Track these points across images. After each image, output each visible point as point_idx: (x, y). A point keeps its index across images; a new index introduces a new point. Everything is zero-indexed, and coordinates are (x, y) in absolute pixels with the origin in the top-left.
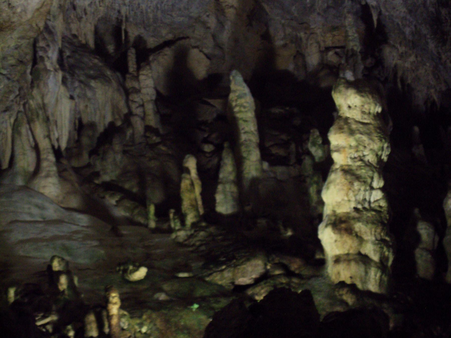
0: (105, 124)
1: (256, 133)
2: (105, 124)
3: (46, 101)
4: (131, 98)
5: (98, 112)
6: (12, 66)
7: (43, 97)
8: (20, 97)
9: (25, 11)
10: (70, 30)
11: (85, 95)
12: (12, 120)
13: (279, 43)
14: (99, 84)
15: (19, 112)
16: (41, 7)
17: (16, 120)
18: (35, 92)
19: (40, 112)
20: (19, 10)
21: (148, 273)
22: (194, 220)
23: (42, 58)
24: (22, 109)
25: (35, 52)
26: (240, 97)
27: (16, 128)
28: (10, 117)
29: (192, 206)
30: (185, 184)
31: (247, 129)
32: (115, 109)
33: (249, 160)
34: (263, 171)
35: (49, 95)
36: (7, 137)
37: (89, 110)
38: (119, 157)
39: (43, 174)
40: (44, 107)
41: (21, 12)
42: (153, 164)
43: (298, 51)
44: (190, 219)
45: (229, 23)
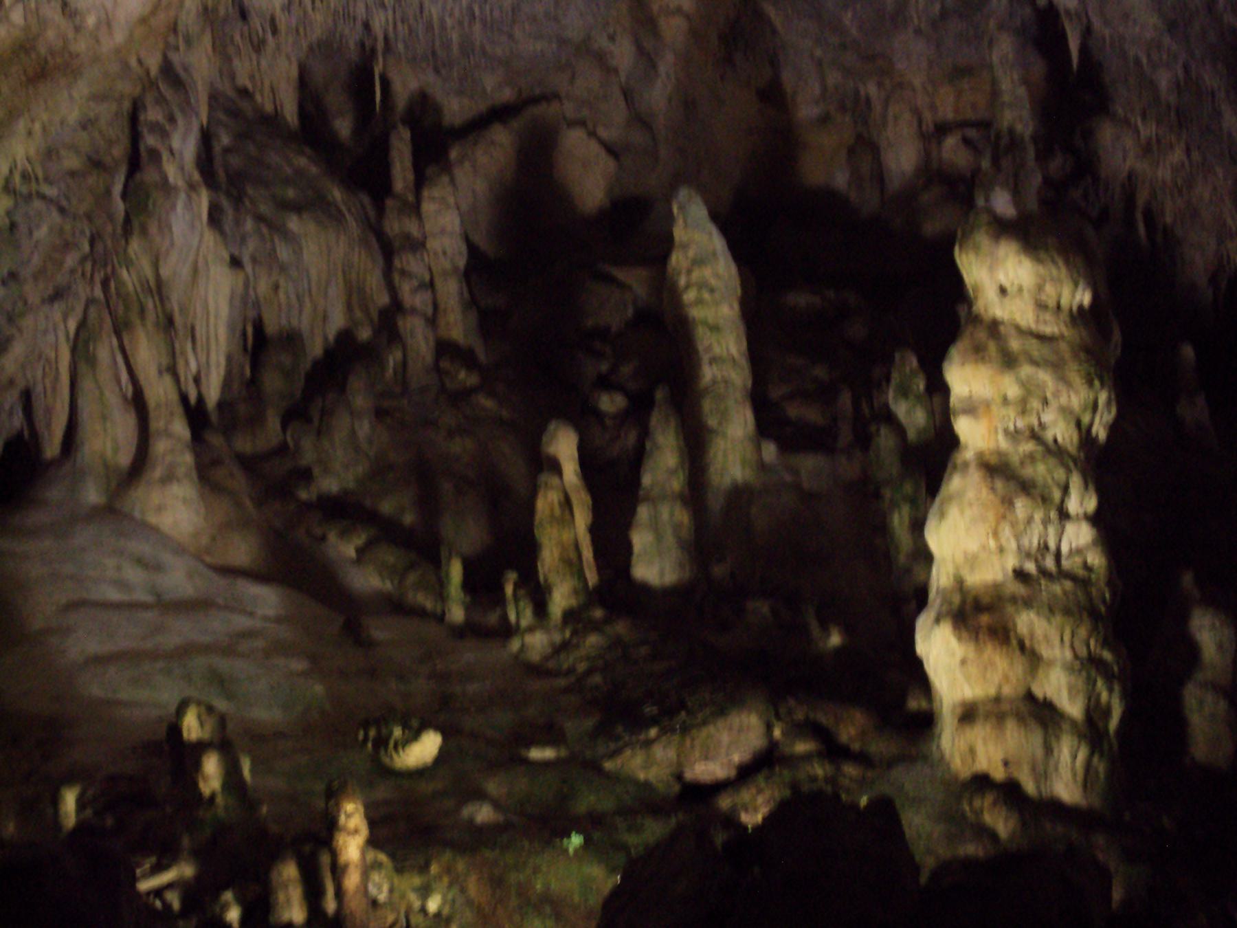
0: (326, 338)
1: (744, 363)
2: (326, 338)
3: (165, 272)
4: (397, 263)
5: (308, 306)
6: (72, 174)
7: (156, 265)
8: (94, 263)
9: (107, 23)
10: (233, 77)
11: (273, 254)
12: (72, 325)
13: (806, 111)
14: (312, 227)
15: (90, 302)
16: (153, 12)
17: (82, 325)
18: (135, 246)
19: (150, 305)
20: (91, 21)
21: (442, 750)
22: (573, 602)
23: (155, 155)
24: (98, 293)
25: (135, 137)
26: (698, 262)
27: (81, 347)
28: (65, 318)
29: (567, 562)
30: (546, 502)
31: (717, 350)
32: (355, 294)
33: (724, 436)
34: (762, 466)
35: (174, 257)
36: (57, 378)
37: (282, 295)
38: (364, 428)
39: (158, 473)
40: (159, 289)
41: (98, 26)
42: (460, 447)
43: (860, 138)
44: (561, 599)
45: (670, 57)
